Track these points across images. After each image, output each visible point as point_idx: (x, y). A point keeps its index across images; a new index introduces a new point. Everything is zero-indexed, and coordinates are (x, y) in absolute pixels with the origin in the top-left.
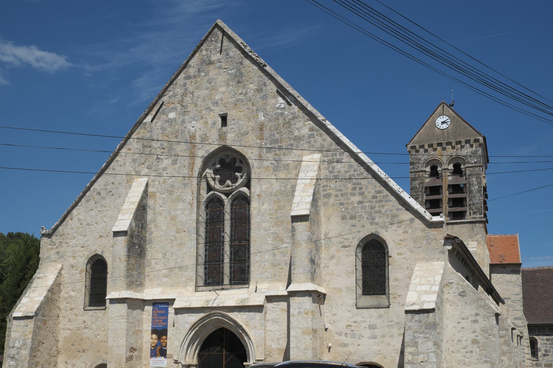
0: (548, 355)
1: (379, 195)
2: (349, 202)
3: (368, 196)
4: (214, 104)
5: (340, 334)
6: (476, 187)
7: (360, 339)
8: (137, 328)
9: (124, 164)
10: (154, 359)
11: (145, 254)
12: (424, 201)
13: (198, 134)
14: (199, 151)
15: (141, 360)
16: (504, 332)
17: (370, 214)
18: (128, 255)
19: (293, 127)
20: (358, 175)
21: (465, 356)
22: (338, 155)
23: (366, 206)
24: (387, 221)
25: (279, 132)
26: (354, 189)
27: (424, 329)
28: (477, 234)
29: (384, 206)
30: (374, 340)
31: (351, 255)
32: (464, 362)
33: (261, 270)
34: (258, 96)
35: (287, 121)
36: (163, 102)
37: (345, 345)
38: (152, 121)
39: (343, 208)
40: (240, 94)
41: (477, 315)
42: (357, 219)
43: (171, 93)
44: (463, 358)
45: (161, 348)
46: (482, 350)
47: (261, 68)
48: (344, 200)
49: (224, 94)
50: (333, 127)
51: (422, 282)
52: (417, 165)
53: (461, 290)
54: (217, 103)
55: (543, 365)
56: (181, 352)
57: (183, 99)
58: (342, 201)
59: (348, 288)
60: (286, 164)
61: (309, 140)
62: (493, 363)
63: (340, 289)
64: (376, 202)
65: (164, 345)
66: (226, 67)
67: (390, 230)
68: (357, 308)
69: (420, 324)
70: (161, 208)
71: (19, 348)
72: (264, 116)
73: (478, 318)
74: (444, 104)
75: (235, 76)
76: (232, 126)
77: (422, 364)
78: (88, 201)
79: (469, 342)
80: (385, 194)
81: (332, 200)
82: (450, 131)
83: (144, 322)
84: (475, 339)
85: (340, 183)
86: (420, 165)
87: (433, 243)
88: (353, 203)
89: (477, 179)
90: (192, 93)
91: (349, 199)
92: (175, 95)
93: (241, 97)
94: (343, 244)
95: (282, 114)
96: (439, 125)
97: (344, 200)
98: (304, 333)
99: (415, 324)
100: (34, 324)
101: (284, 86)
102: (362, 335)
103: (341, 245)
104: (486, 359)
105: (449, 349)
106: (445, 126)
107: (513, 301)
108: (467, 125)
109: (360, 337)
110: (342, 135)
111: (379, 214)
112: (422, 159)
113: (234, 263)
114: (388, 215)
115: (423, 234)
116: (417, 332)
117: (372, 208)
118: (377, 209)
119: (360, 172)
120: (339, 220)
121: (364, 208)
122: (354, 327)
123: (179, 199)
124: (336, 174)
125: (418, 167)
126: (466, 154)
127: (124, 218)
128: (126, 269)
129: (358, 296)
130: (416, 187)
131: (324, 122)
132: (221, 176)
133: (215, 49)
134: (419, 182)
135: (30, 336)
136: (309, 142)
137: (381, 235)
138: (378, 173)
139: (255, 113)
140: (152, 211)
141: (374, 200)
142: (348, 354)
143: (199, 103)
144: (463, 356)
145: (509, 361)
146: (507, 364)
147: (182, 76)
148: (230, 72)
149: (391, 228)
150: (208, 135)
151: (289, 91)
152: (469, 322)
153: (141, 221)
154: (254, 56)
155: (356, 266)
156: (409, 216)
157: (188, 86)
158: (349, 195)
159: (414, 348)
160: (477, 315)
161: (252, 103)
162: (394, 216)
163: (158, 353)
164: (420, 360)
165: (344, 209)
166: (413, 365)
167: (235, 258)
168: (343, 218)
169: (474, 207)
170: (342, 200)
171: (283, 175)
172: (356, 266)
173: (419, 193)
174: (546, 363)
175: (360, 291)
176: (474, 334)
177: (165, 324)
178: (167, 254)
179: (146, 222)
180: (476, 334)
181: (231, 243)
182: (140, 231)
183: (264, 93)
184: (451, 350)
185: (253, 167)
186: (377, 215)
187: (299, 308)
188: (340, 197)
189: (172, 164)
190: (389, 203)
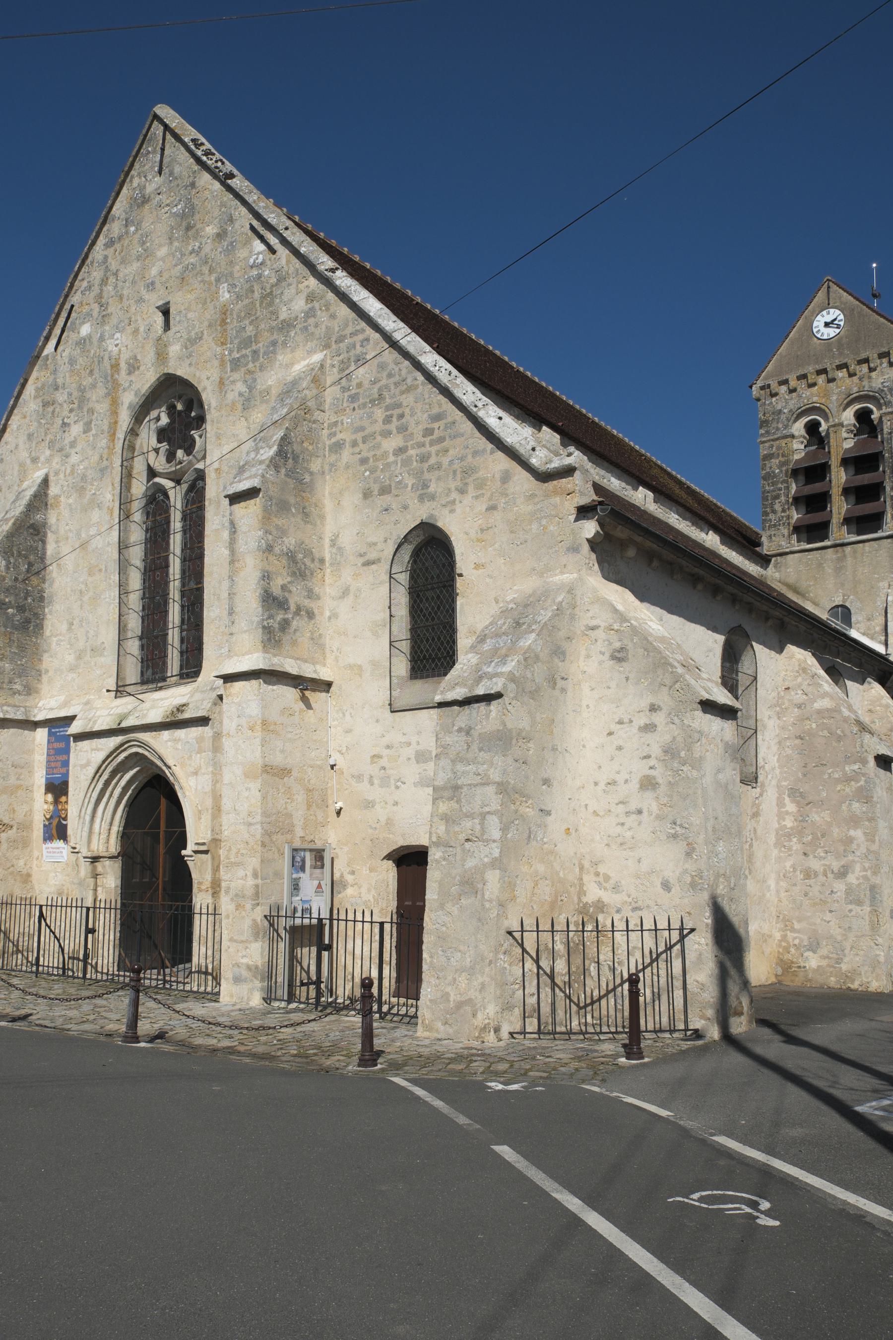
1: (436, 425)
2: (378, 453)
3: (415, 431)
4: (148, 287)
5: (359, 778)
8: (12, 780)
9: (17, 447)
10: (49, 845)
11: (40, 627)
12: (791, 500)
13: (124, 357)
15: (29, 849)
17: (418, 474)
19: (278, 301)
20: (395, 384)
21: (623, 824)
22: (358, 347)
23: (411, 456)
24: (452, 486)
25: (253, 320)
26: (388, 420)
27: (477, 750)
29: (447, 451)
31: (381, 583)
32: (620, 840)
33: (219, 637)
34: (220, 250)
35: (269, 291)
36: (72, 306)
37: (369, 805)
39: (366, 471)
40: (191, 253)
41: (653, 708)
42: (394, 492)
44: (619, 829)
45: (59, 821)
46: (665, 805)
47: (224, 180)
48: (369, 451)
49: (164, 262)
52: (774, 425)
53: (617, 645)
54: (153, 283)
56: (79, 830)
57: (101, 290)
58: (364, 454)
59: (375, 664)
60: (264, 390)
62: (690, 840)
64: (431, 445)
65: (63, 816)
66: (168, 202)
67: (458, 508)
68: (392, 712)
70: (67, 527)
72: (229, 292)
74: (831, 283)
75: (183, 216)
76: (177, 329)
77: (468, 845)
79: (634, 785)
80: (450, 419)
81: (346, 455)
83: (36, 768)
84: (648, 776)
85: (362, 412)
86: (780, 426)
88: (385, 454)
90: (116, 274)
91: (378, 446)
93: (193, 259)
94: (367, 558)
95: (260, 276)
96: (819, 331)
97: (369, 451)
98: (247, 775)
102: (402, 780)
103: (361, 560)
104: (673, 831)
105: (586, 805)
106: (832, 332)
108: (882, 320)
111: (437, 472)
112: (785, 411)
113: (187, 630)
114: (455, 472)
116: (462, 760)
117: (424, 458)
118: (433, 461)
119: (400, 375)
121: (406, 463)
122: (385, 759)
124: (353, 392)
125: (778, 429)
126: (880, 386)
129: (394, 680)
130: (773, 472)
132: (169, 444)
133: (152, 168)
134: (780, 462)
136: (306, 328)
137: (440, 524)
139: (213, 288)
140: (54, 536)
142: (374, 826)
143: (125, 292)
144: (618, 824)
145: (867, 841)
146: (863, 849)
147: (102, 240)
148: (175, 209)
149: (461, 502)
150: (139, 358)
151: (269, 220)
155: (390, 608)
156: (502, 461)
157: (109, 260)
158: (379, 438)
159: (454, 804)
160: (653, 708)
161: (208, 268)
163: (54, 832)
165: (367, 473)
166: (448, 849)
167: (189, 618)
168: (367, 494)
170: (364, 449)
171: (259, 415)
172: (390, 608)
173: (780, 485)
175: (402, 666)
176: (645, 761)
177: (63, 770)
178: (75, 622)
179: (43, 558)
180: (652, 762)
184: (591, 809)
185: (209, 410)
186: (432, 476)
187: (239, 717)
188: (361, 445)
190: (459, 440)
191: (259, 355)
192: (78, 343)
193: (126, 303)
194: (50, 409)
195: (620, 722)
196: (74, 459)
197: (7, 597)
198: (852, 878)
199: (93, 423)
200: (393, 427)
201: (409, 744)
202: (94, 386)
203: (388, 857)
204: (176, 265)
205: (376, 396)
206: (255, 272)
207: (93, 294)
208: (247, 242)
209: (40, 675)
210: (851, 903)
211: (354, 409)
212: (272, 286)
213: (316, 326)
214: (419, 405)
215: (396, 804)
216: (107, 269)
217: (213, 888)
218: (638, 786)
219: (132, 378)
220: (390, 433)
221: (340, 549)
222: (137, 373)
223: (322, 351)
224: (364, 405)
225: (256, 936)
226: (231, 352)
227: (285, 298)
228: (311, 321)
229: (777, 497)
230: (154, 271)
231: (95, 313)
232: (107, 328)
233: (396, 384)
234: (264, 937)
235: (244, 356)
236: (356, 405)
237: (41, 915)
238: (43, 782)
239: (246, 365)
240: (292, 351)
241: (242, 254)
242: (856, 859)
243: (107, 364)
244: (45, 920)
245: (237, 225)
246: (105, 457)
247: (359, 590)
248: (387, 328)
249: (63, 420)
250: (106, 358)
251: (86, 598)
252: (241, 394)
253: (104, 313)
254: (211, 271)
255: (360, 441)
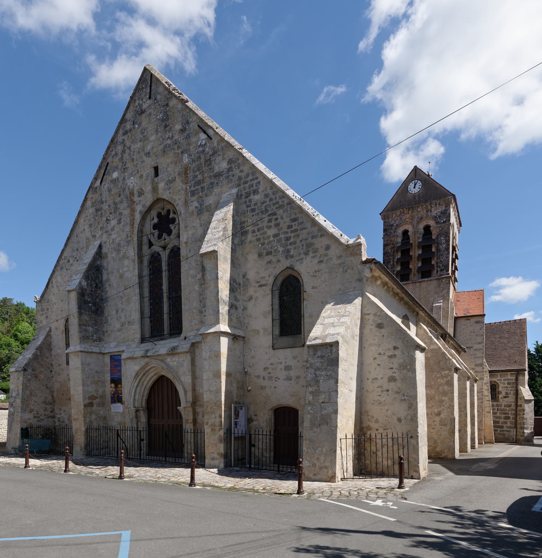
0: (508, 397)
1: (293, 224)
2: (266, 236)
3: (283, 226)
5: (258, 377)
6: (444, 246)
7: (276, 381)
10: (114, 405)
11: (102, 312)
13: (136, 189)
14: (138, 206)
16: (446, 372)
18: (78, 312)
21: (380, 395)
22: (254, 186)
23: (282, 238)
24: (302, 252)
26: (270, 221)
27: (326, 366)
28: (443, 289)
30: (290, 382)
31: (268, 294)
32: (379, 402)
34: (182, 137)
36: (108, 163)
38: (101, 184)
39: (259, 244)
41: (395, 348)
43: (113, 153)
45: (118, 395)
48: (261, 235)
50: (250, 154)
51: (332, 314)
52: (390, 231)
53: (379, 322)
54: (149, 153)
55: (503, 405)
58: (259, 237)
59: (265, 330)
61: (228, 175)
63: (258, 331)
65: (120, 393)
67: (305, 262)
69: (322, 361)
71: (15, 398)
73: (397, 352)
75: (163, 120)
77: (323, 405)
78: (62, 268)
79: (386, 379)
82: (421, 195)
87: (349, 271)
88: (269, 237)
89: (445, 238)
90: (129, 148)
91: (266, 233)
92: (116, 154)
93: (169, 142)
94: (260, 284)
97: (261, 235)
99: (316, 361)
100: (23, 377)
101: (203, 119)
102: (279, 378)
104: (403, 398)
107: (475, 350)
109: (277, 379)
110: (259, 161)
112: (395, 225)
115: (339, 262)
117: (288, 239)
120: (256, 256)
121: (279, 241)
123: (125, 257)
124: (252, 207)
125: (391, 233)
126: (435, 215)
127: (76, 278)
128: (78, 325)
129: (274, 336)
130: (388, 251)
131: (240, 151)
133: (145, 95)
135: (21, 387)
136: (228, 177)
138: (292, 197)
139: (180, 156)
141: (289, 230)
143: (135, 157)
151: (208, 123)
152: (386, 357)
153: (95, 280)
154: (177, 94)
155: (272, 305)
158: (266, 229)
159: (315, 388)
160: (395, 348)
162: (309, 245)
163: (116, 399)
164: (321, 401)
165: (260, 245)
167: (173, 309)
168: (260, 255)
169: (441, 265)
174: (506, 404)
175: (277, 332)
179: (101, 282)
180: (394, 370)
181: (170, 294)
182: (93, 290)
183: (187, 132)
188: (257, 233)
189: (118, 224)
191: (205, 189)
192: (112, 181)
193: (135, 162)
194: (100, 213)
195: (380, 354)
196: (114, 236)
197: (88, 298)
198: (442, 416)
199: (122, 220)
200: (272, 224)
201: (281, 363)
202: (121, 202)
203: (271, 410)
204: (160, 145)
205: (264, 210)
206: (201, 149)
207: (118, 158)
208: (197, 133)
209: (104, 333)
210: (442, 425)
211: (253, 215)
212: (210, 156)
213: (233, 176)
214: (285, 214)
215: (276, 387)
216: (125, 146)
217: (193, 422)
218: (387, 380)
219: (140, 198)
220: (271, 227)
221: (247, 279)
222: (143, 196)
223: (236, 188)
224: (258, 214)
225: (221, 441)
226: (190, 187)
227: (217, 161)
228: (231, 173)
229: (389, 262)
230: (149, 147)
231: (120, 167)
232: (126, 174)
233: (274, 204)
234: (224, 442)
235: (197, 189)
236: (254, 214)
237: (118, 434)
238: (109, 378)
239: (198, 194)
240: (221, 187)
241: (194, 140)
242: (445, 408)
243: (127, 192)
244: (120, 437)
245: (191, 125)
246: (129, 235)
247: (257, 297)
248: (270, 177)
249: (107, 218)
250: (127, 189)
251: (124, 300)
252: (196, 207)
253: (124, 167)
254: (178, 148)
255: (256, 230)
